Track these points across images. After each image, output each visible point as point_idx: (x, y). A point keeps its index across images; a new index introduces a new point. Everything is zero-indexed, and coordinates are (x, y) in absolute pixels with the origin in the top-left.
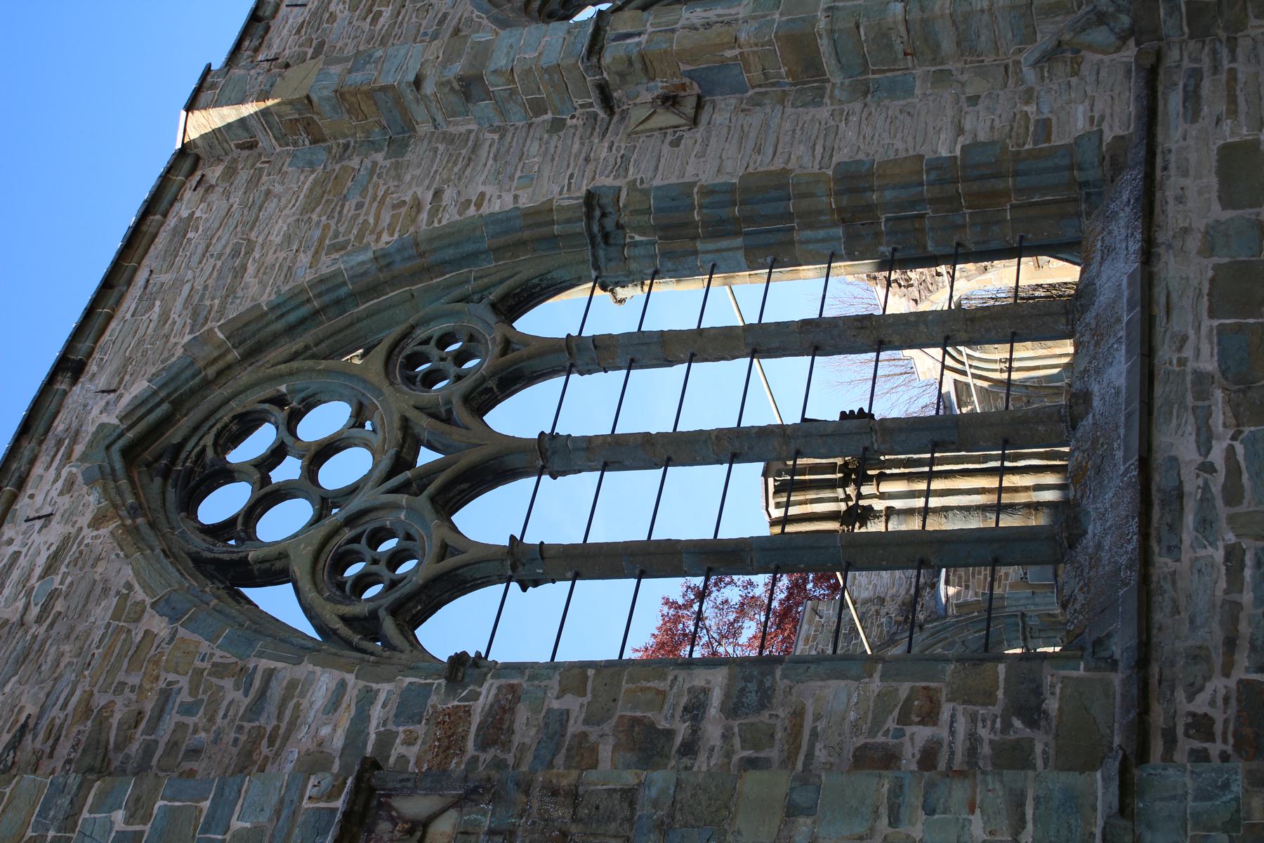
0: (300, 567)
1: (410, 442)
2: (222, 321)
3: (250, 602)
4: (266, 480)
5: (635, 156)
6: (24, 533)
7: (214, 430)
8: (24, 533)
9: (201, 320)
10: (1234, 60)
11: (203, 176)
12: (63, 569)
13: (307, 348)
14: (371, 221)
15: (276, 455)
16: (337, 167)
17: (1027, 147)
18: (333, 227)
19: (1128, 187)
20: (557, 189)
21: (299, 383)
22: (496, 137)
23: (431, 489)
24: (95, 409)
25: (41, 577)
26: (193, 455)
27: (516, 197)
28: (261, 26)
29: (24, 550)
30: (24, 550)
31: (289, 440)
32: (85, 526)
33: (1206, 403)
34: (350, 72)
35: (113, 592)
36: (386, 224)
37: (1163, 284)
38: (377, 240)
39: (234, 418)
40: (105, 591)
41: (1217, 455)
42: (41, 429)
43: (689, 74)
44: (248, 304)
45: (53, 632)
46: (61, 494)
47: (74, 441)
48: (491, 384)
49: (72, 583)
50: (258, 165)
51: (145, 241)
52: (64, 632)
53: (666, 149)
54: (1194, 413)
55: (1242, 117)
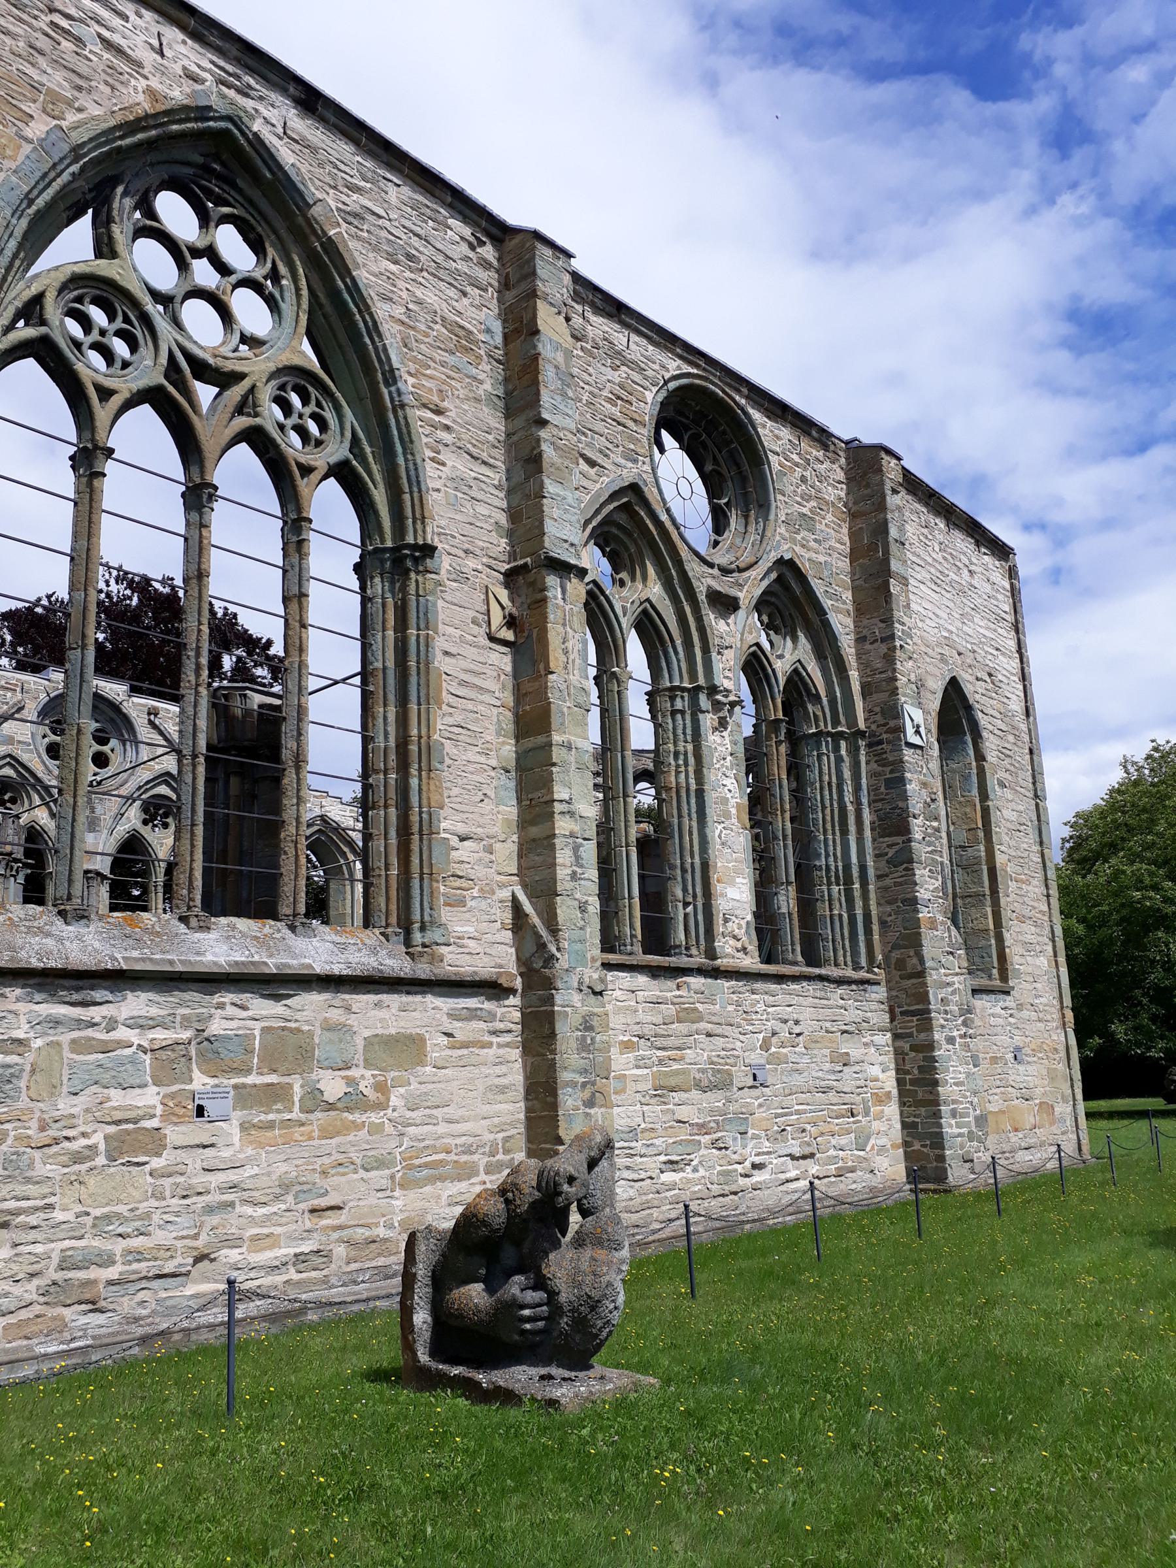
0: (105, 268)
1: (223, 379)
2: (346, 236)
3: (70, 221)
4: (197, 253)
5: (466, 588)
6: (147, 29)
7: (250, 218)
8: (147, 29)
9: (350, 219)
10: (500, 1046)
11: (485, 243)
12: (106, 55)
13: (321, 306)
14: (428, 372)
15: (223, 269)
16: (482, 352)
17: (442, 888)
18: (426, 340)
19: (394, 962)
20: (443, 523)
21: (290, 295)
22: (496, 482)
23: (171, 389)
24: (271, 119)
25: (99, 35)
26: (226, 195)
27: (438, 490)
28: (614, 311)
29: (129, 25)
30: (129, 25)
31: (233, 279)
32: (149, 83)
33: (178, 1025)
34: (556, 367)
35: (76, 94)
36: (424, 382)
37: (110, 997)
38: (410, 374)
39: (260, 236)
40: (79, 88)
41: (122, 1033)
42: (250, 62)
43: (529, 636)
44: (360, 260)
45: (39, 35)
46: (184, 68)
47: (239, 91)
48: (272, 454)
49: (91, 60)
50: (490, 289)
51: (427, 184)
52: (38, 44)
53: (472, 614)
54: (169, 1015)
55: (449, 1052)
